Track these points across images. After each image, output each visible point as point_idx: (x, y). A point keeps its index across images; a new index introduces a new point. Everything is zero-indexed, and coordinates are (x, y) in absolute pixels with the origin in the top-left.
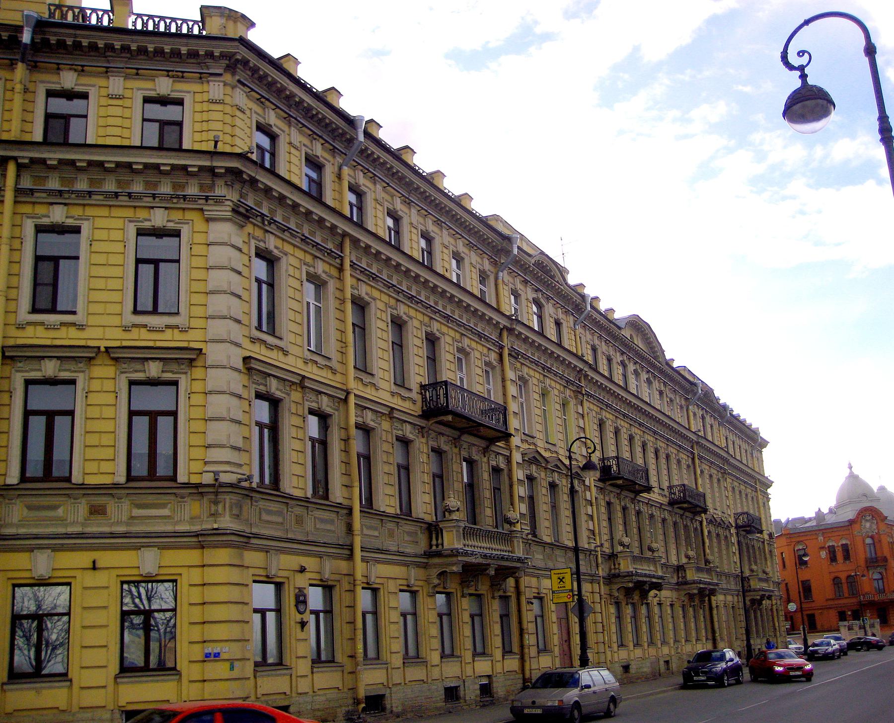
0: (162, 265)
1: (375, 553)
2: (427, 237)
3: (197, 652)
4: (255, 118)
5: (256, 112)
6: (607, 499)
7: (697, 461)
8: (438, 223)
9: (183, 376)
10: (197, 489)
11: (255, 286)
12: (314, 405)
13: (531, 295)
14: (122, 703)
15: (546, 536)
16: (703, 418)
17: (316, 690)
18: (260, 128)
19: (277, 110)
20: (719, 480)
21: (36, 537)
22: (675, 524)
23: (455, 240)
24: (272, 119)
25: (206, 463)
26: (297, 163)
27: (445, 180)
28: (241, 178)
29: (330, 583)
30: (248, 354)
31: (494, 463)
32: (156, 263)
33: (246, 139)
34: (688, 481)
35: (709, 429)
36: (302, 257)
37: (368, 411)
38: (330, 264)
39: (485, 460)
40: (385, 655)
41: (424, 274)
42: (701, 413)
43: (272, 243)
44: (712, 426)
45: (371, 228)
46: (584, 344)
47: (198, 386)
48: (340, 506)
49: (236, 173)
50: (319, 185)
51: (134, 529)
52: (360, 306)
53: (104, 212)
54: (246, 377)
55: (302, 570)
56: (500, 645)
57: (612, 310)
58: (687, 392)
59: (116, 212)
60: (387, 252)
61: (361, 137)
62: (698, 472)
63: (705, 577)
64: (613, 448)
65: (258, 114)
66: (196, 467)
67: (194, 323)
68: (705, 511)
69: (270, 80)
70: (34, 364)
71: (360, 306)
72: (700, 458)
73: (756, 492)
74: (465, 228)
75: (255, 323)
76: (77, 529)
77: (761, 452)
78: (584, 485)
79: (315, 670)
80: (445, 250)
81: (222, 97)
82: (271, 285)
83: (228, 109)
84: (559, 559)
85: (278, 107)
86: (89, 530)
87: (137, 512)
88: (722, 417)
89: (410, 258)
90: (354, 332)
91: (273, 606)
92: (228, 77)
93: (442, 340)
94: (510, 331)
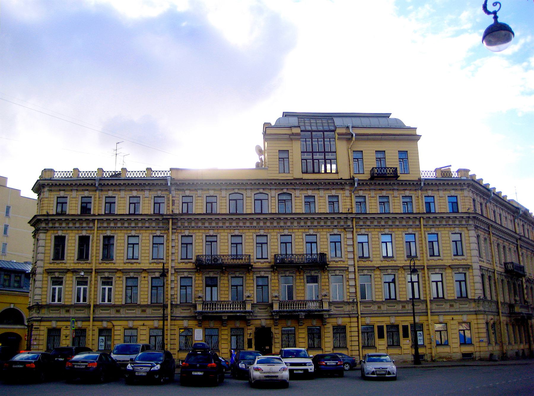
3: (477, 340)
7: (519, 249)
10: (474, 300)
16: (523, 225)
21: (440, 312)
22: (508, 282)
34: (515, 260)
35: (526, 232)
42: (522, 223)
44: (528, 230)
47: (471, 274)
49: (474, 217)
51: (461, 310)
53: (443, 229)
57: (488, 184)
58: (514, 212)
59: (446, 229)
61: (492, 195)
62: (520, 254)
63: (524, 311)
66: (473, 295)
67: (468, 258)
68: (524, 276)
70: (128, 273)
72: (521, 246)
73: (489, 234)
76: (448, 310)
86: (451, 310)
87: (461, 306)
88: (489, 196)
92: (468, 189)
94: (520, 239)
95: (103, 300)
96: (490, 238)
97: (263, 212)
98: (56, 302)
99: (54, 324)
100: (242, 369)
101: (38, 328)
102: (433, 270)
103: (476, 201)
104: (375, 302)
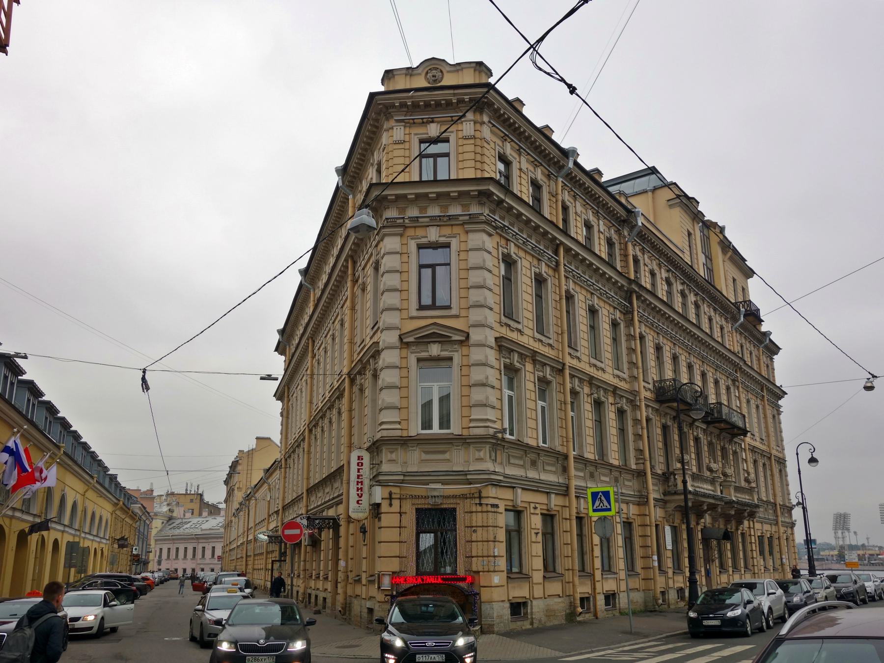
0: (438, 268)
2: (588, 226)
6: (663, 421)
8: (596, 214)
9: (455, 353)
13: (664, 275)
15: (614, 458)
19: (512, 143)
20: (728, 388)
24: (509, 150)
25: (471, 420)
26: (526, 185)
28: (487, 198)
29: (520, 509)
30: (498, 335)
32: (433, 267)
33: (494, 169)
39: (691, 432)
41: (583, 254)
45: (573, 235)
50: (508, 177)
52: (569, 297)
56: (541, 567)
64: (714, 396)
71: (509, 262)
77: (772, 359)
80: (578, 218)
81: (472, 133)
83: (478, 142)
85: (513, 141)
89: (576, 241)
95: (427, 424)
97: (438, 179)
98: (436, 429)
100: (227, 655)
103: (714, 321)
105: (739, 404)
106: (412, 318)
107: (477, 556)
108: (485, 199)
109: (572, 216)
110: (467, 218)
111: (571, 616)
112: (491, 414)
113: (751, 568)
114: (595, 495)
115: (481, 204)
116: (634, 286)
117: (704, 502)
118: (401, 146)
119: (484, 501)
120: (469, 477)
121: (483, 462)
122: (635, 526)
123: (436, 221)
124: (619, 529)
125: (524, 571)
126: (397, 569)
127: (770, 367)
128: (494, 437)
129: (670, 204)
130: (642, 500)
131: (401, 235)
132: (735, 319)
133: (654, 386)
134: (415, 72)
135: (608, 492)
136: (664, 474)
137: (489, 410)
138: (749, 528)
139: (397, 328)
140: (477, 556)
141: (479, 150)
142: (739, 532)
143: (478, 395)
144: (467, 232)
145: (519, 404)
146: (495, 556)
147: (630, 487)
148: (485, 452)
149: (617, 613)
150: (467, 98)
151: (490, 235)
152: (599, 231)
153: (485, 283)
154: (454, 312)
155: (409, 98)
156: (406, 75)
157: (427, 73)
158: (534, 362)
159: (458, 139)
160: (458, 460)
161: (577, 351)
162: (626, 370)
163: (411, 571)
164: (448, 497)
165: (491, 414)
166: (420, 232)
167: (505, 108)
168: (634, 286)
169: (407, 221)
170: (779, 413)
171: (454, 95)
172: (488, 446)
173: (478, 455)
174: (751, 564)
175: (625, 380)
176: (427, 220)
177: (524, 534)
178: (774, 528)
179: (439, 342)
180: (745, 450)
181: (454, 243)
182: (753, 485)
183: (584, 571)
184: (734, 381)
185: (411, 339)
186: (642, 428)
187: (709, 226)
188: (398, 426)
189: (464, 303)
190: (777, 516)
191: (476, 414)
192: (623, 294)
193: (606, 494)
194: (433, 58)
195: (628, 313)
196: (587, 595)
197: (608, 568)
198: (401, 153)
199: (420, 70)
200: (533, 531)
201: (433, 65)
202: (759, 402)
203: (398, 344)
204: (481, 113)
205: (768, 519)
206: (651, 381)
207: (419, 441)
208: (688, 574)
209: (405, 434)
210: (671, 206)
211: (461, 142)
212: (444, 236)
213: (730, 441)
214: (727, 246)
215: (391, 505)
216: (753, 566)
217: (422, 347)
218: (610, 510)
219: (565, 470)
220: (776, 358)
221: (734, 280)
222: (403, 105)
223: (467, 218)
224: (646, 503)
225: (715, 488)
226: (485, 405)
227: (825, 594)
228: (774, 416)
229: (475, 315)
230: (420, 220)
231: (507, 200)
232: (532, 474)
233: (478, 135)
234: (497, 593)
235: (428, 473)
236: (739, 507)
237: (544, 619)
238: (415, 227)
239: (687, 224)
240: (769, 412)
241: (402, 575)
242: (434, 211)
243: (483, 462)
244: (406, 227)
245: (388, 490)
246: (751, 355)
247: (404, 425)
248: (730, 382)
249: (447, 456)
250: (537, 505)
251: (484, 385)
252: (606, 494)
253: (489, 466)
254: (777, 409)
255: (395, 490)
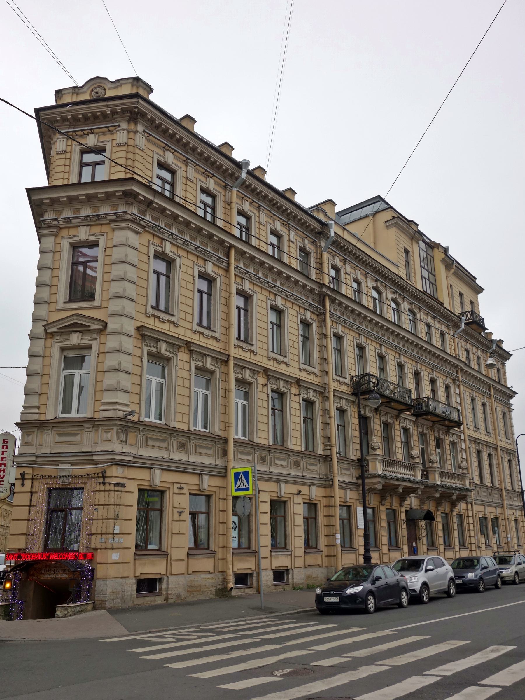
1: (510, 507)
4: (269, 226)
5: (200, 180)
9: (94, 342)
11: (197, 295)
12: (275, 387)
14: (138, 574)
17: (306, 566)
18: (204, 191)
23: (355, 271)
27: (196, 125)
30: (140, 324)
31: (403, 425)
36: (298, 309)
37: (207, 357)
38: (219, 267)
40: (380, 545)
43: (280, 302)
46: (460, 348)
48: (498, 488)
54: (140, 341)
55: (299, 493)
60: (426, 346)
65: (271, 224)
69: (176, 135)
74: (444, 317)
75: (196, 320)
78: (460, 439)
79: (273, 553)
81: (125, 140)
82: (246, 311)
83: (131, 149)
84: (484, 494)
90: (273, 329)
91: (204, 510)
93: (422, 374)
96: (491, 403)
99: (159, 478)
101: (123, 485)
102: (153, 343)
104: (175, 430)
105: (462, 402)
106: (59, 310)
107: (96, 534)
108: (131, 200)
109: (471, 355)
110: (114, 217)
111: (223, 592)
112: (122, 398)
113: (468, 546)
114: (237, 475)
115: (128, 204)
116: (324, 290)
117: (399, 485)
118: (63, 156)
119: (107, 481)
120: (94, 457)
121: (111, 443)
122: (320, 507)
123: (89, 221)
124: (266, 507)
125: (163, 549)
126: (22, 546)
127: (501, 372)
128: (124, 419)
129: (388, 224)
130: (328, 483)
131: (56, 236)
132: (457, 326)
133: (351, 380)
134: (81, 90)
135: (247, 472)
136: (358, 460)
137: (119, 394)
138: (467, 510)
139: (44, 320)
140: (96, 534)
141: (130, 156)
142: (454, 513)
143: (110, 380)
144: (114, 230)
145: (169, 390)
146: (114, 534)
147: (317, 470)
148: (112, 434)
149: (288, 588)
150: (119, 109)
151: (138, 233)
152: (290, 241)
153: (125, 275)
154: (97, 303)
155: (68, 112)
156: (73, 93)
157: (92, 91)
158: (191, 352)
159: (112, 146)
160: (89, 442)
161: (252, 345)
162: (316, 365)
163: (37, 547)
164: (75, 477)
165: (122, 398)
166: (72, 232)
167: (160, 119)
168: (324, 290)
169: (61, 222)
170: (510, 410)
171: (108, 106)
172: (115, 428)
173: (105, 436)
174: (468, 542)
175: (314, 374)
176: (79, 220)
177: (166, 512)
178: (499, 511)
179: (80, 331)
180: (465, 441)
181: (102, 244)
182: (465, 471)
183: (246, 547)
184: (454, 380)
185: (54, 330)
186: (330, 417)
187: (432, 246)
188: (37, 411)
189: (106, 296)
190: (503, 500)
191: (108, 397)
192: (317, 298)
193: (246, 474)
194: (97, 78)
195: (321, 314)
196: (249, 571)
197: (279, 543)
198: (62, 162)
199: (85, 89)
200: (176, 511)
201: (97, 82)
202: (485, 400)
203: (43, 334)
204: (136, 123)
205: (493, 502)
206: (348, 377)
207: (55, 424)
208: (362, 550)
209: (42, 418)
210: (388, 227)
211: (115, 149)
212: (93, 235)
213: (447, 433)
214: (450, 263)
215: (23, 485)
216: (471, 544)
217: (65, 337)
218: (248, 489)
219: (225, 453)
220: (508, 363)
221: (461, 295)
222: (64, 119)
223: (114, 217)
224: (332, 486)
225: (415, 472)
226: (116, 389)
227: (514, 570)
228: (504, 414)
229: (115, 306)
230: (73, 221)
231: (156, 201)
232: (177, 456)
233: (131, 142)
234: (117, 569)
235: (59, 455)
236: (444, 490)
237: (183, 594)
238: (69, 228)
239: (406, 243)
240: (500, 410)
241: (28, 551)
242: (86, 212)
243: (111, 443)
244: (61, 228)
245: (21, 470)
246: (480, 362)
247: (42, 410)
248: (449, 381)
249: (78, 438)
250: (183, 486)
251: (116, 370)
252: (246, 474)
253: (117, 447)
254: (509, 407)
255: (29, 471)
